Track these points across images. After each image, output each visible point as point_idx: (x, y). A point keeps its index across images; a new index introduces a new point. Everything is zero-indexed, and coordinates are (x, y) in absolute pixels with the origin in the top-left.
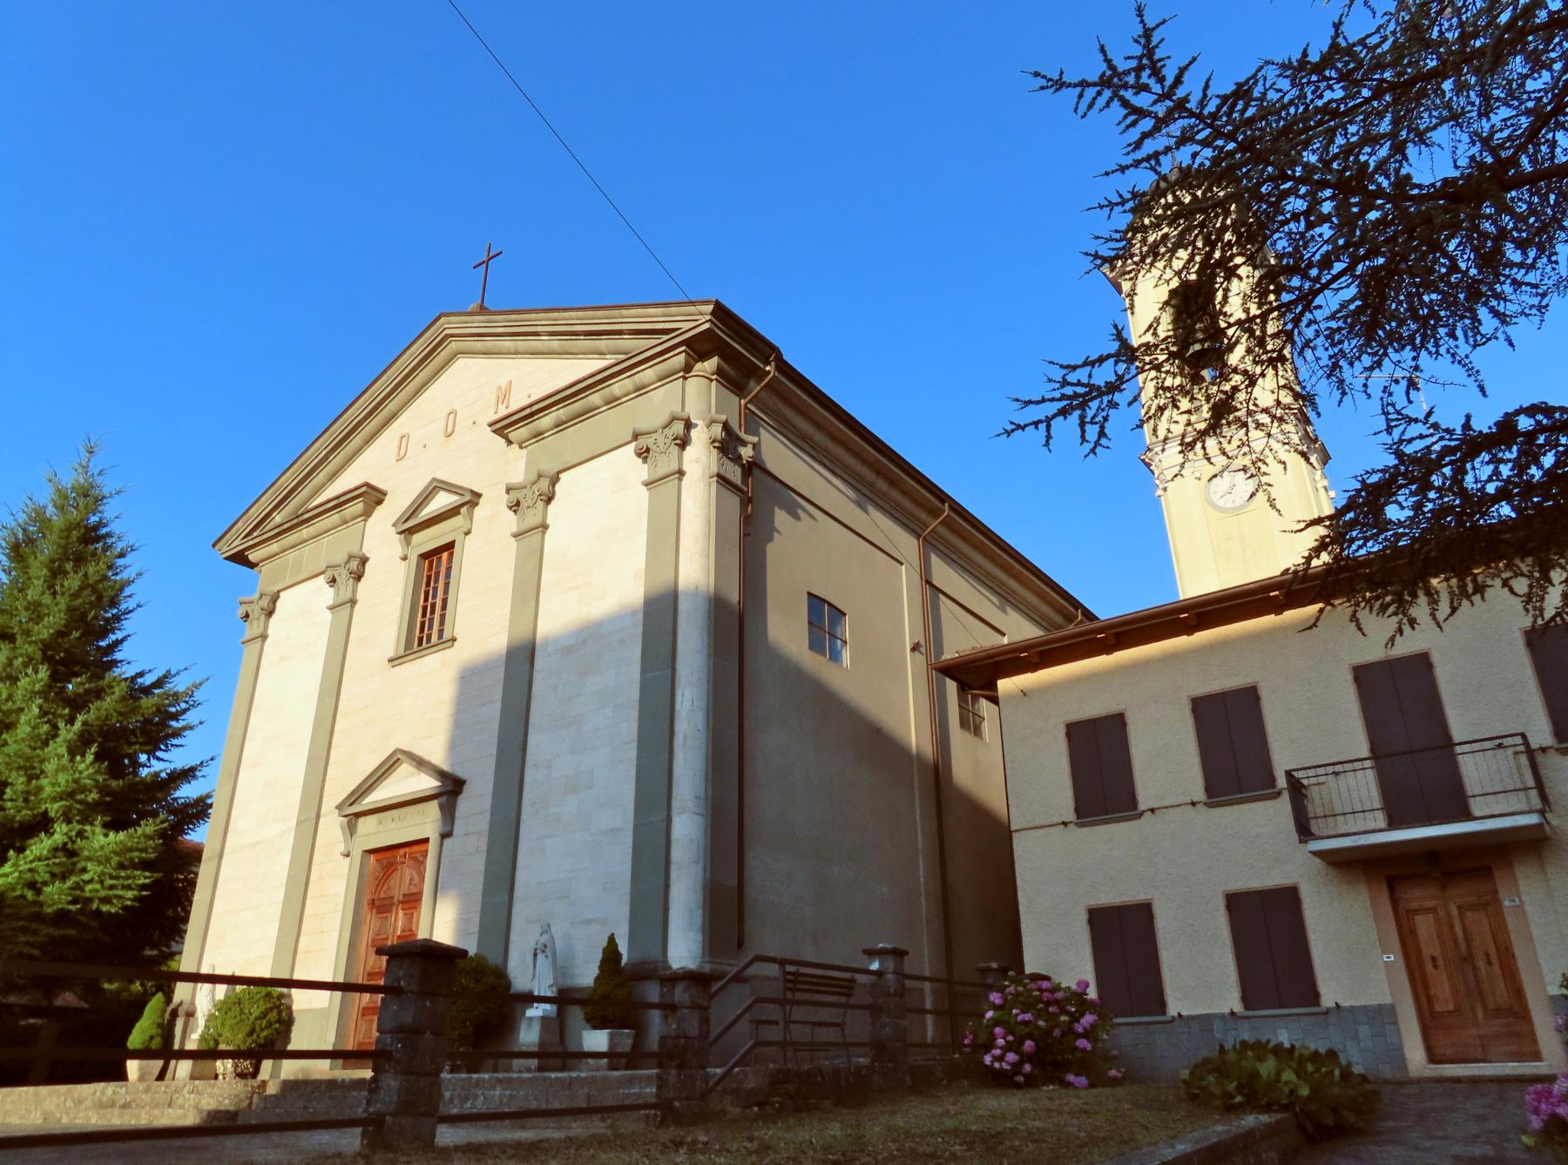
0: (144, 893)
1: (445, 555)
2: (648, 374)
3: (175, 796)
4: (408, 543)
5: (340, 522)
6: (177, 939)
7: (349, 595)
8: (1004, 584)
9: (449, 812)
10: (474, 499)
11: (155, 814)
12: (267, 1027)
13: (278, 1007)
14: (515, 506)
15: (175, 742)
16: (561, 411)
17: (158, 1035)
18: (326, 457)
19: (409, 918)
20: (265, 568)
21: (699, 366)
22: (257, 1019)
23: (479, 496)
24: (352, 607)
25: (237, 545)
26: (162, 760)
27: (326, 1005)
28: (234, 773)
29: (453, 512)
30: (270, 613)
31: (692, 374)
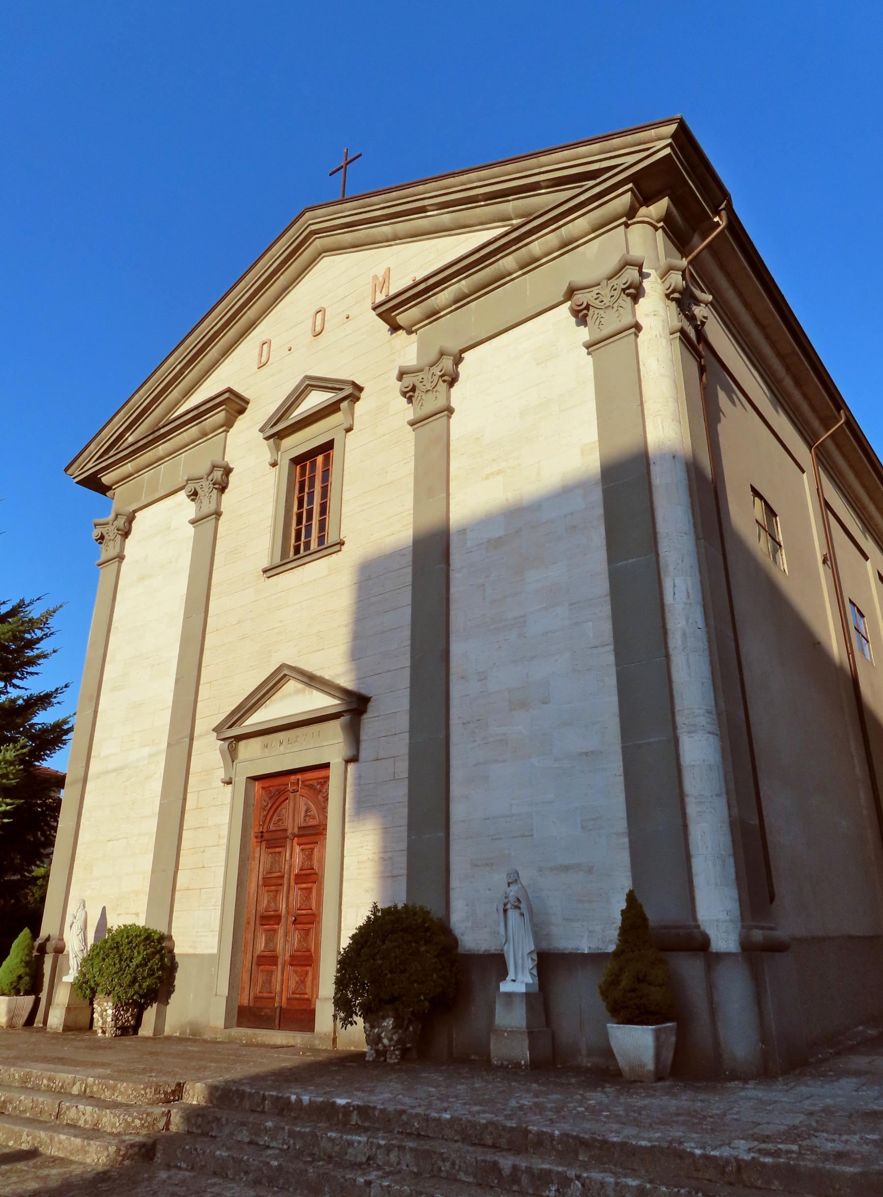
0: (6, 821)
1: (320, 459)
2: (580, 224)
3: (32, 721)
4: (278, 448)
5: (200, 435)
6: (38, 863)
7: (213, 507)
8: (865, 508)
9: (354, 733)
10: (355, 392)
11: (15, 741)
12: (150, 976)
13: (160, 951)
14: (409, 394)
15: (30, 669)
16: (463, 282)
17: (27, 974)
18: (181, 372)
19: (309, 856)
20: (119, 492)
21: (643, 210)
22: (137, 966)
23: (360, 389)
24: (217, 519)
25: (91, 468)
26: (18, 687)
27: (215, 951)
28: (95, 695)
29: (332, 409)
30: (126, 534)
31: (635, 220)
